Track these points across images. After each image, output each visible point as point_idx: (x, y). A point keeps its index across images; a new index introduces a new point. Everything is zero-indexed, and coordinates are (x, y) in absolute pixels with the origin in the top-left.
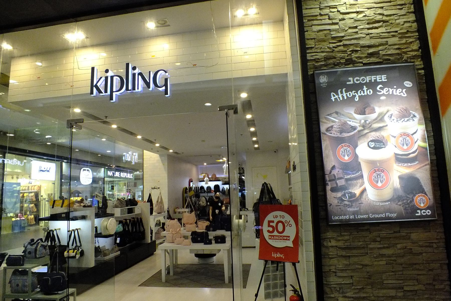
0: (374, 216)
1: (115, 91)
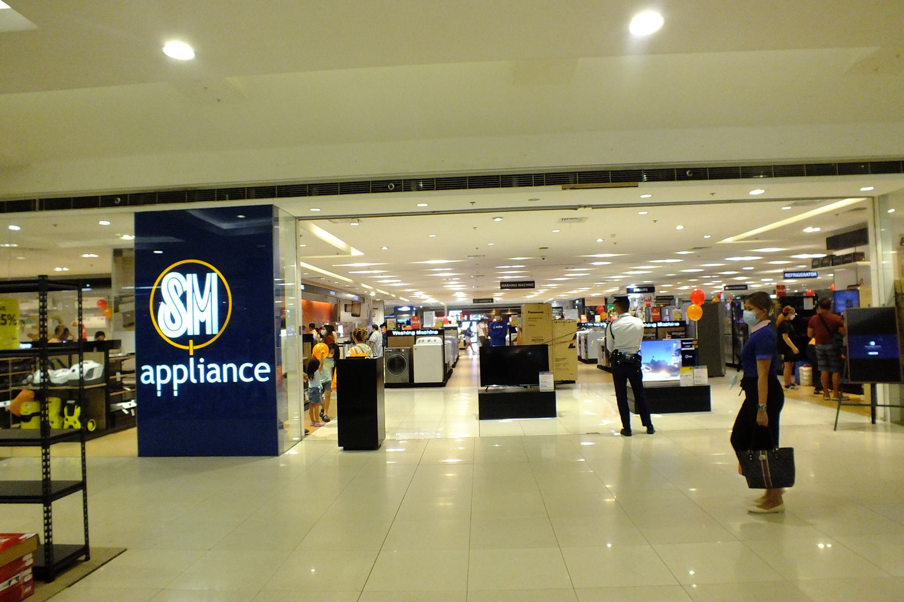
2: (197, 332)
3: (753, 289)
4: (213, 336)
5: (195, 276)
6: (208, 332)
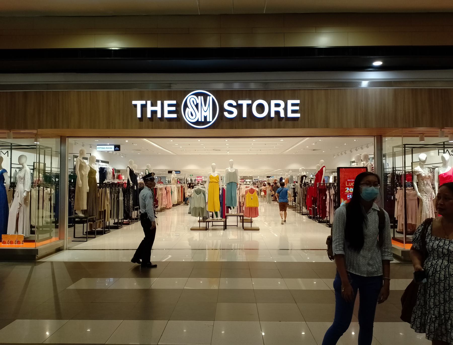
2: (203, 120)
4: (210, 122)
5: (202, 97)
6: (208, 120)
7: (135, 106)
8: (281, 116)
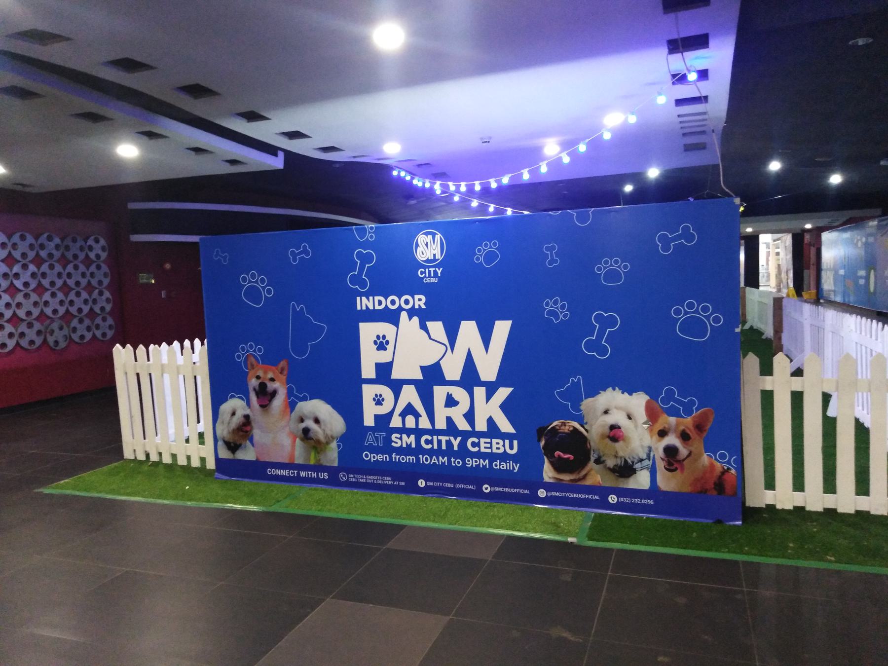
0: (399, 458)
1: (490, 450)
2: (432, 258)
3: (234, 508)
5: (431, 236)
6: (437, 258)
7: (475, 465)
8: (496, 321)
